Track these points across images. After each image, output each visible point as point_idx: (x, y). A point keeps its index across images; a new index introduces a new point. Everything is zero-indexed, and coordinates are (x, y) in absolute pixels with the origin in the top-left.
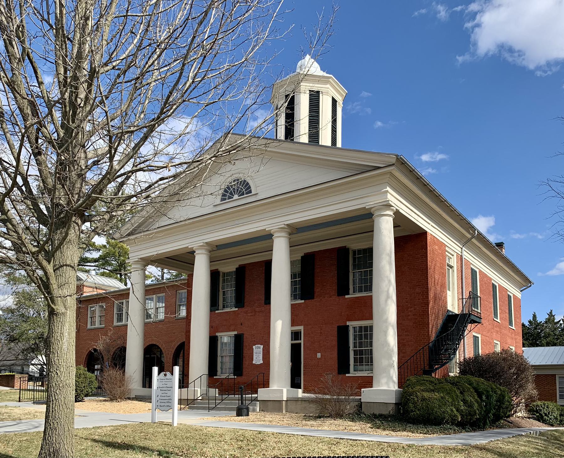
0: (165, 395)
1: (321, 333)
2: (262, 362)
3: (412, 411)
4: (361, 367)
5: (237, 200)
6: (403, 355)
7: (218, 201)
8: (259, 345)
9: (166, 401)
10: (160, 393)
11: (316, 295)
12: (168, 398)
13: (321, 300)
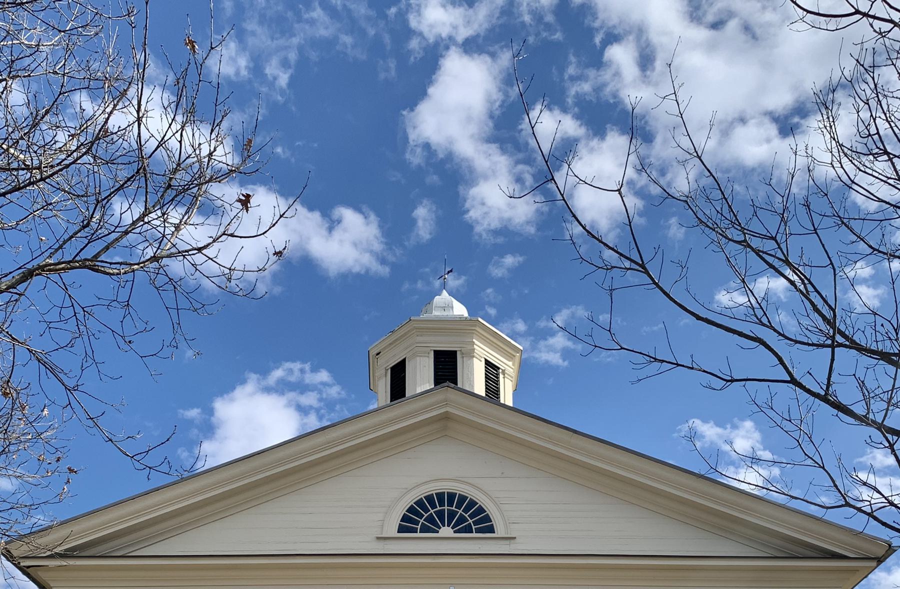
5: (446, 539)
7: (392, 529)
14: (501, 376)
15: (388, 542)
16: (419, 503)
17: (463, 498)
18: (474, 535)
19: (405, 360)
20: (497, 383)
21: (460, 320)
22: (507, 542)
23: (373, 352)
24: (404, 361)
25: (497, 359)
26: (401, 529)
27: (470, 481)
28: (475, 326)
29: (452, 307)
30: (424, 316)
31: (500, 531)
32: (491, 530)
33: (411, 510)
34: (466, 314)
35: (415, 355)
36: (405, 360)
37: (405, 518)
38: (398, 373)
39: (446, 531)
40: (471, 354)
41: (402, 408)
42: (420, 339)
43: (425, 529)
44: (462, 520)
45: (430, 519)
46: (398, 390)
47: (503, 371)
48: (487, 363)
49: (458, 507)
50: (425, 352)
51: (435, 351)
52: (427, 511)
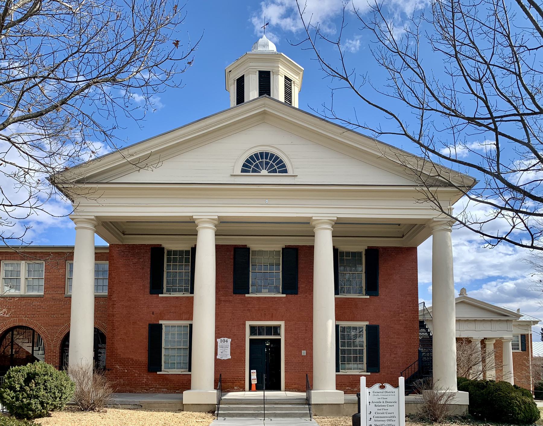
0: (385, 411)
1: (306, 330)
2: (229, 357)
3: (518, 414)
4: (347, 366)
5: (264, 177)
6: (394, 356)
7: (238, 171)
8: (226, 339)
9: (386, 419)
10: (374, 409)
11: (300, 290)
12: (389, 415)
13: (306, 296)
14: (293, 85)
15: (235, 177)
16: (251, 157)
17: (272, 155)
18: (278, 174)
19: (244, 75)
20: (291, 89)
21: (272, 54)
22: (293, 178)
23: (227, 71)
24: (243, 76)
25: (291, 75)
26: (243, 171)
27: (276, 146)
28: (280, 57)
29: (268, 45)
30: (253, 52)
31: (290, 172)
32: (286, 171)
33: (247, 161)
34: (275, 50)
35: (249, 74)
36: (244, 75)
37: (244, 165)
38: (240, 82)
39: (264, 172)
40: (277, 73)
41: (242, 108)
42: (251, 64)
43: (254, 171)
44: (272, 166)
45: (257, 166)
46: (240, 99)
47: (294, 82)
48: (286, 78)
49: (270, 160)
50: (254, 72)
51: (260, 72)
52: (255, 161)
